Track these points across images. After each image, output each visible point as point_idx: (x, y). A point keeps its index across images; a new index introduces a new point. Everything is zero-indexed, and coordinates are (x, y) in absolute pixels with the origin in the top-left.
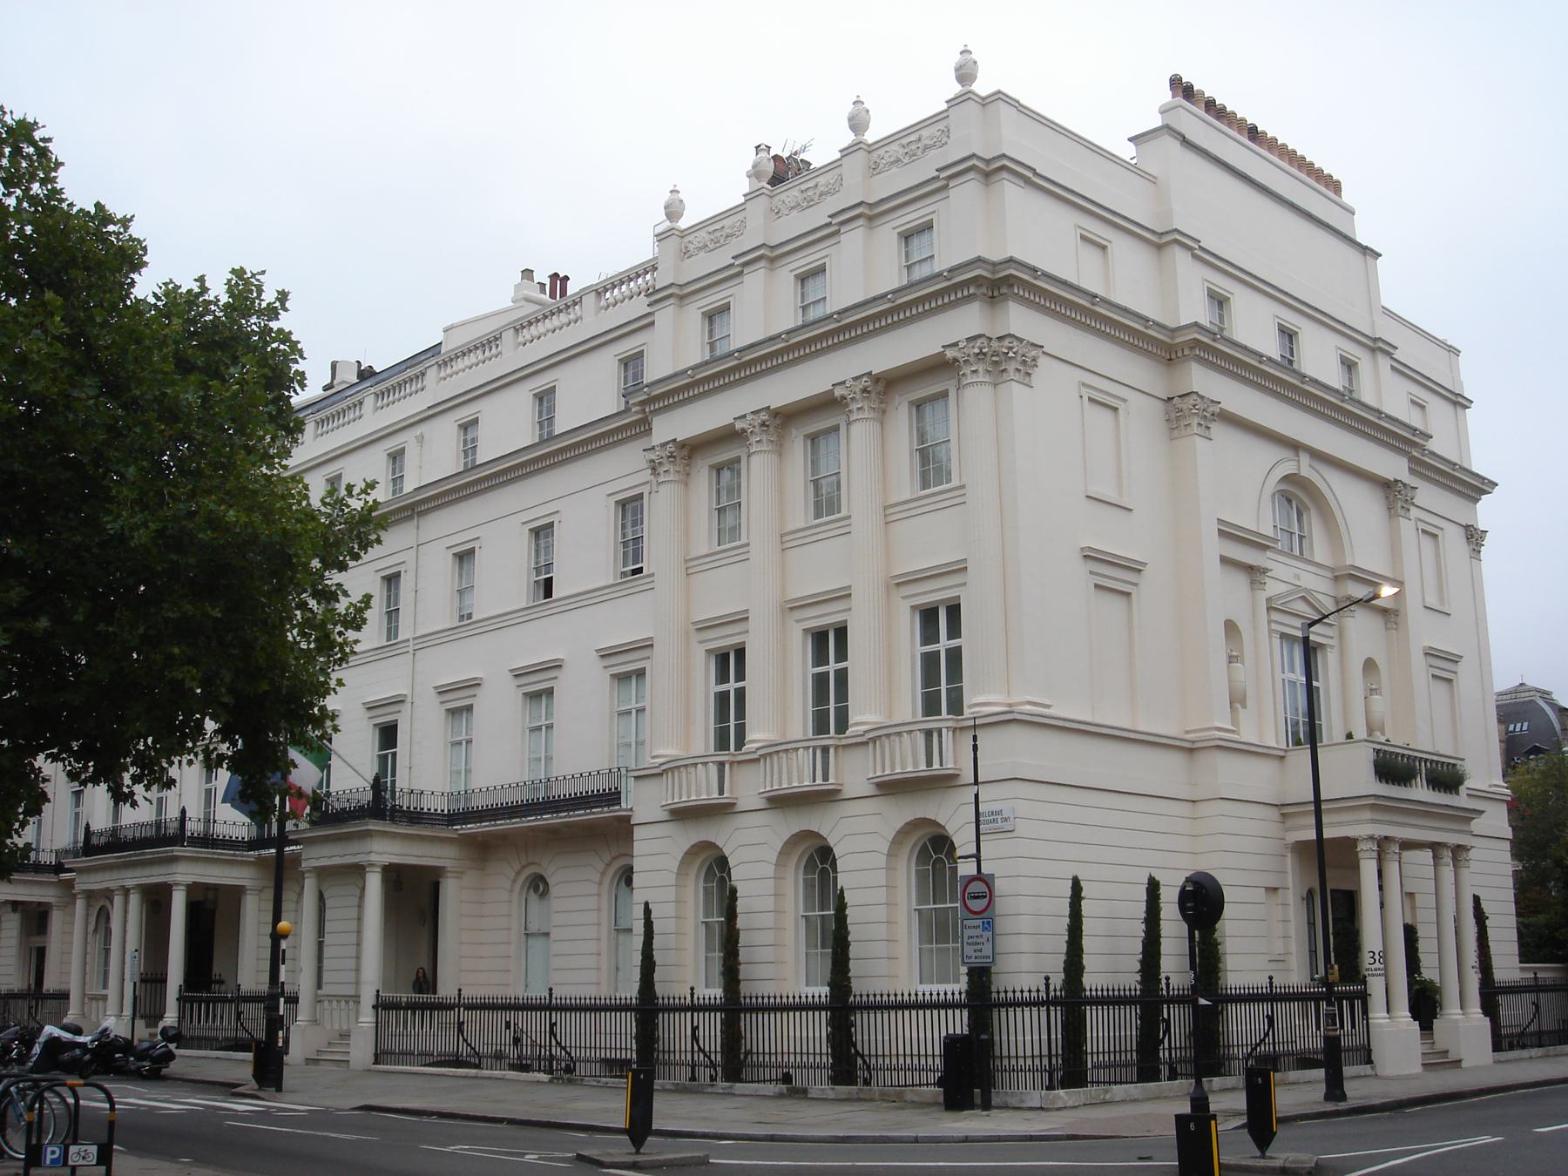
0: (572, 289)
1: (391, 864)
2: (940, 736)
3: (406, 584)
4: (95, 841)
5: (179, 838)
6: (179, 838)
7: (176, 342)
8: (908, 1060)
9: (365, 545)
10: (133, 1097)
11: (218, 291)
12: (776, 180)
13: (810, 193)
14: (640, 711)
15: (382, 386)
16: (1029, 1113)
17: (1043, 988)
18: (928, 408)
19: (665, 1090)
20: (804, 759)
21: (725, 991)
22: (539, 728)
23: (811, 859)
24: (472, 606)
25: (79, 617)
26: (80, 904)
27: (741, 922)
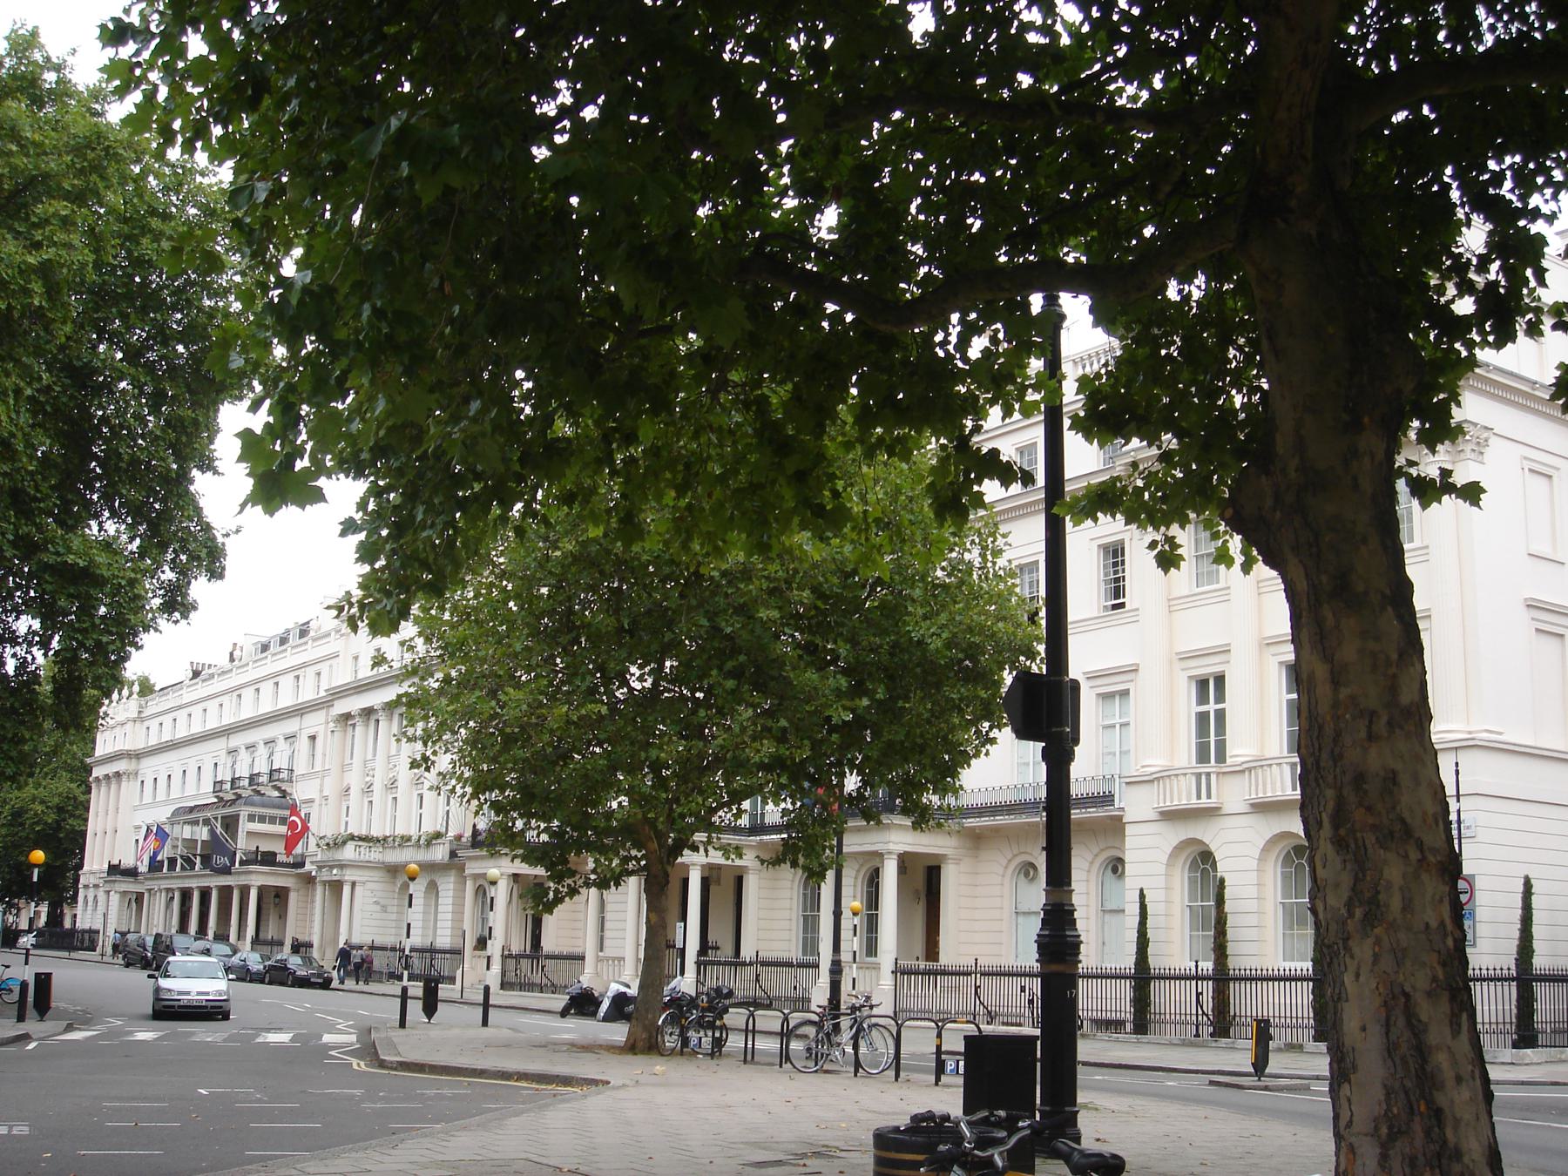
19: (1279, 1050)
23: (1194, 862)
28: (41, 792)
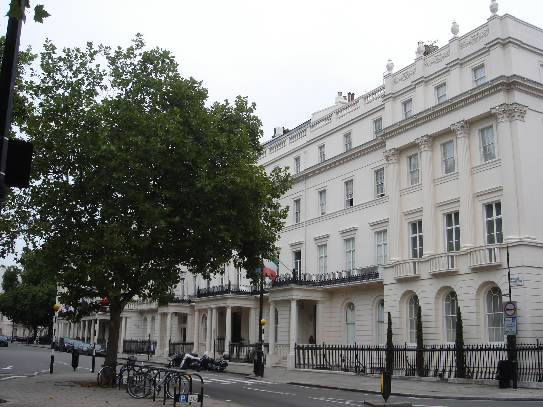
0: (356, 97)
1: (300, 299)
2: (495, 251)
3: (302, 203)
4: (201, 292)
5: (228, 291)
6: (228, 291)
7: (218, 122)
8: (485, 369)
9: (286, 189)
10: (210, 378)
11: (232, 104)
12: (426, 54)
13: (439, 57)
14: (385, 244)
15: (292, 135)
16: (528, 391)
17: (536, 343)
18: (486, 132)
19: (396, 379)
20: (444, 260)
21: (418, 343)
22: (350, 251)
23: (448, 296)
24: (325, 210)
25: (189, 216)
26: (197, 313)
27: (423, 319)
28: (43, 289)
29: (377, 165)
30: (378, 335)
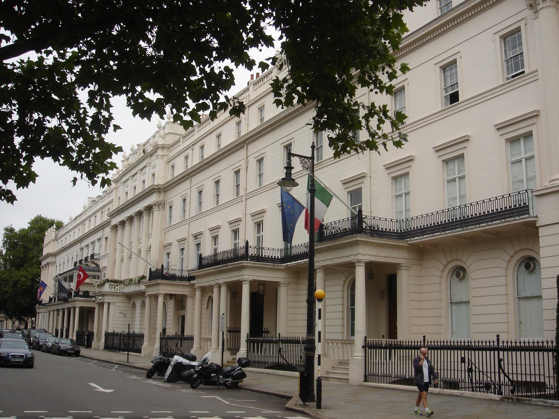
5: (246, 256)
6: (246, 256)
22: (454, 180)
26: (198, 293)
28: (25, 273)
29: (507, 25)
30: (518, 322)
